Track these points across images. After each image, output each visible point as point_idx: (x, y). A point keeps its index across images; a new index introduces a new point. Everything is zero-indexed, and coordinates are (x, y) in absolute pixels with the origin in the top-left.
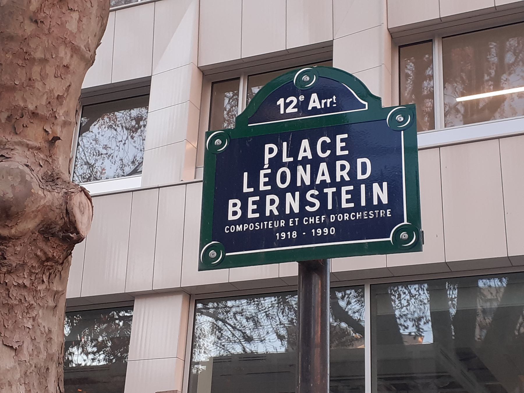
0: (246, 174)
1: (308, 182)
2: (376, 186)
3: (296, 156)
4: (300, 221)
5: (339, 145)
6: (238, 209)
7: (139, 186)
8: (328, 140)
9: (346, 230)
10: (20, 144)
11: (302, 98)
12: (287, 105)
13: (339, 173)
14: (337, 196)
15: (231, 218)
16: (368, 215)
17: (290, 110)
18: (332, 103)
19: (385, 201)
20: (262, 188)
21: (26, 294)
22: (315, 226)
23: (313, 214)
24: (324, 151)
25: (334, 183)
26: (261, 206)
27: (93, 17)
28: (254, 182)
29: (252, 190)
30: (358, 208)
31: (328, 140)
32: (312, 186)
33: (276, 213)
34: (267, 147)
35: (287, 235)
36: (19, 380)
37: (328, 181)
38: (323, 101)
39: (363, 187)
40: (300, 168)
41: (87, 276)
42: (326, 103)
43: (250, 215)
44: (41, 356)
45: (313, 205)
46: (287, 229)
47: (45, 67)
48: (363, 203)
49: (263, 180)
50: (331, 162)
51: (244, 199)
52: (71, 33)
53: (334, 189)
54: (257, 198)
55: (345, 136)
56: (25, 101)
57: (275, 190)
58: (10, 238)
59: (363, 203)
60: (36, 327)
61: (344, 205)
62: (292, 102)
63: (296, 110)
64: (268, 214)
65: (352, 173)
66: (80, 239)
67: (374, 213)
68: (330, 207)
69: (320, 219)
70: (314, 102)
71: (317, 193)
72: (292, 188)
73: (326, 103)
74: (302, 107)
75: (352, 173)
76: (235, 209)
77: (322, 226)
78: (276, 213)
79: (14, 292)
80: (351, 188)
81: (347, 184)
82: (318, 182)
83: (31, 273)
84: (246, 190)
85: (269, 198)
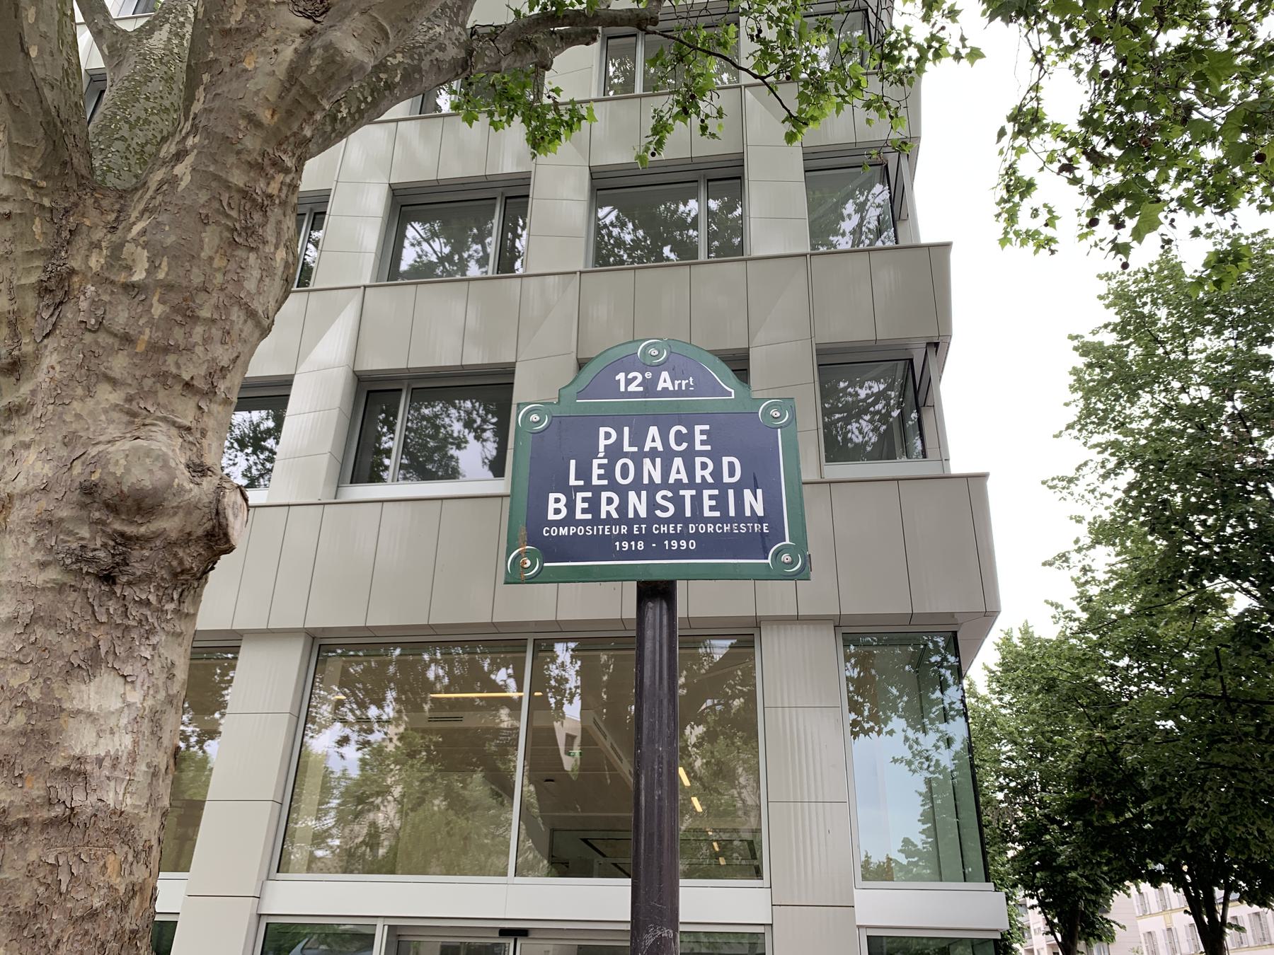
0: (573, 463)
1: (658, 480)
2: (747, 493)
3: (641, 447)
4: (649, 529)
5: (699, 438)
6: (561, 505)
7: (263, 502)
8: (684, 431)
9: (709, 545)
10: (165, 419)
11: (648, 375)
12: (629, 382)
13: (699, 473)
14: (697, 501)
15: (551, 516)
16: (739, 529)
17: (632, 388)
18: (688, 385)
19: (760, 513)
20: (595, 482)
21: (149, 613)
22: (669, 537)
23: (667, 521)
24: (678, 444)
25: (691, 484)
26: (594, 506)
27: (277, 278)
28: (584, 473)
29: (581, 483)
30: (725, 518)
31: (684, 431)
32: (665, 484)
33: (615, 515)
34: (602, 430)
35: (630, 546)
36: (126, 728)
37: (685, 481)
38: (677, 382)
39: (731, 492)
40: (647, 462)
41: (223, 601)
42: (680, 385)
43: (579, 516)
44: (158, 697)
45: (665, 509)
46: (630, 537)
47: (210, 329)
48: (732, 513)
49: (596, 472)
50: (689, 457)
51: (570, 492)
52: (249, 293)
53: (693, 492)
54: (589, 494)
55: (707, 427)
56: (178, 366)
57: (613, 486)
58: (138, 539)
59: (732, 513)
60: (156, 658)
61: (707, 513)
62: (635, 378)
63: (641, 389)
64: (603, 516)
65: (717, 473)
66: (230, 549)
67: (747, 527)
68: (688, 514)
69: (675, 529)
70: (665, 381)
71: (670, 494)
72: (637, 486)
73: (680, 385)
74: (649, 387)
75: (717, 473)
76: (557, 506)
77: (678, 537)
78: (615, 515)
79: (134, 611)
80: (716, 492)
81: (711, 487)
82: (671, 481)
83: (158, 587)
84: (573, 482)
85: (604, 495)
